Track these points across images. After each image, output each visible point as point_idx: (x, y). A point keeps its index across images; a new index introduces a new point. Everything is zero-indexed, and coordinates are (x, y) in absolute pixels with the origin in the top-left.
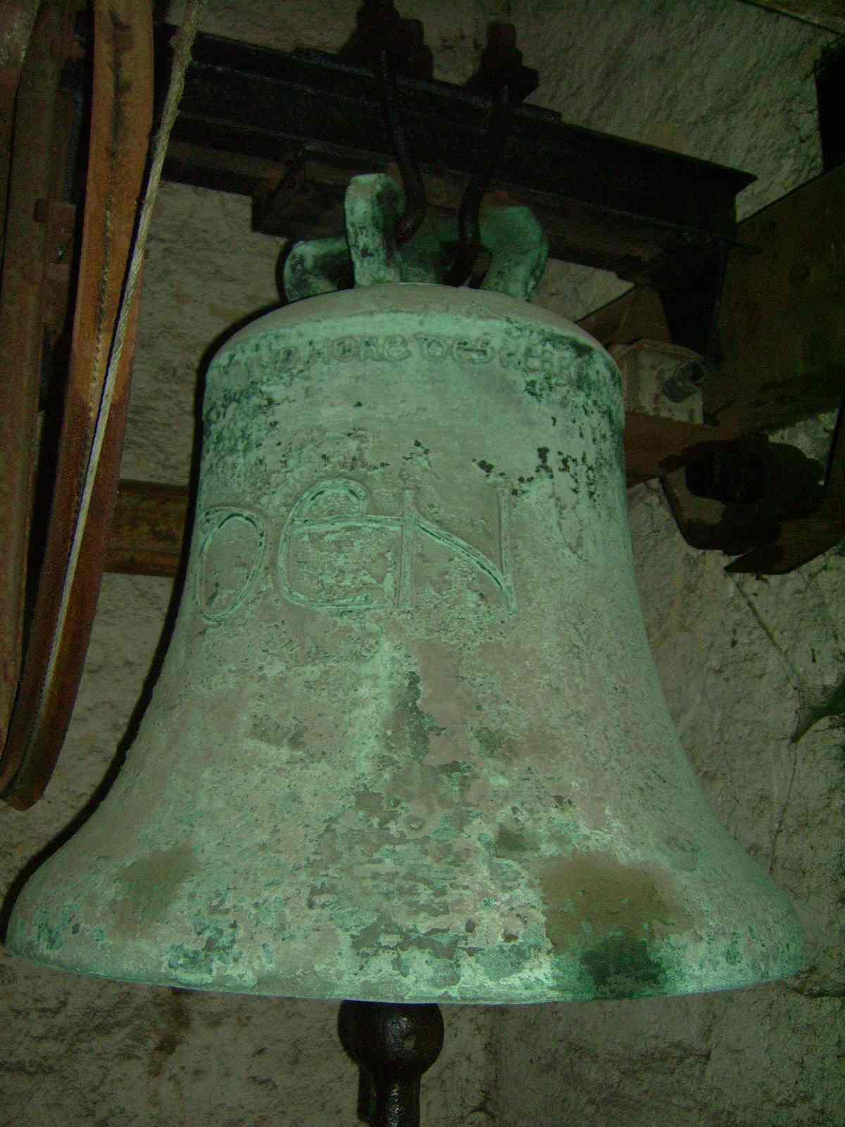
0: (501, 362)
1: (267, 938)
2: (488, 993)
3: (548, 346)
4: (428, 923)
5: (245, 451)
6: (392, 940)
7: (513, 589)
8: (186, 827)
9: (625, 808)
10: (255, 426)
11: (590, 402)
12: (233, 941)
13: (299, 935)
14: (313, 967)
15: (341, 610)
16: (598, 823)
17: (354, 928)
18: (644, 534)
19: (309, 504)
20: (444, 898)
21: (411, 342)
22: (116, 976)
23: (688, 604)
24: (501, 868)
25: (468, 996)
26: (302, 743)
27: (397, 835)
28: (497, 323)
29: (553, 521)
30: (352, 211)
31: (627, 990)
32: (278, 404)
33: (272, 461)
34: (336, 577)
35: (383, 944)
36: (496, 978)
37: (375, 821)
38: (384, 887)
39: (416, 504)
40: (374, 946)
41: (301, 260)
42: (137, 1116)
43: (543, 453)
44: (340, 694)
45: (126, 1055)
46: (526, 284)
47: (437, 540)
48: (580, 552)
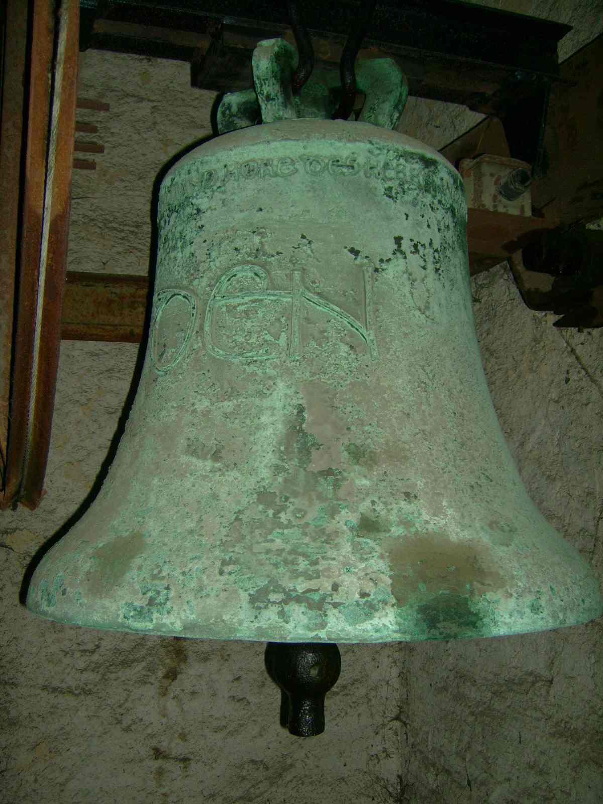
0: (365, 174)
1: (190, 597)
2: (347, 635)
3: (402, 161)
4: (304, 585)
5: (182, 247)
6: (278, 597)
7: (375, 341)
8: (140, 519)
9: (459, 501)
10: (189, 229)
11: (436, 202)
12: (167, 599)
13: (213, 594)
14: (222, 617)
15: (249, 361)
16: (437, 511)
17: (251, 589)
18: (503, 302)
19: (225, 285)
20: (317, 567)
21: (298, 162)
22: (89, 625)
23: (535, 352)
24: (360, 545)
25: (333, 637)
26: (221, 457)
27: (286, 522)
28: (362, 145)
29: (406, 290)
30: (258, 67)
31: (453, 634)
32: (204, 212)
33: (201, 255)
34: (245, 337)
35: (271, 600)
36: (353, 624)
37: (271, 512)
38: (275, 559)
39: (303, 280)
40: (265, 602)
41: (229, 107)
42: (152, 723)
43: (398, 240)
44: (248, 421)
45: (143, 682)
46: (391, 116)
47: (318, 307)
48: (427, 313)
